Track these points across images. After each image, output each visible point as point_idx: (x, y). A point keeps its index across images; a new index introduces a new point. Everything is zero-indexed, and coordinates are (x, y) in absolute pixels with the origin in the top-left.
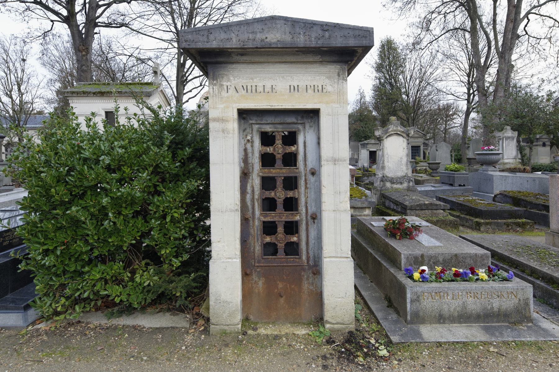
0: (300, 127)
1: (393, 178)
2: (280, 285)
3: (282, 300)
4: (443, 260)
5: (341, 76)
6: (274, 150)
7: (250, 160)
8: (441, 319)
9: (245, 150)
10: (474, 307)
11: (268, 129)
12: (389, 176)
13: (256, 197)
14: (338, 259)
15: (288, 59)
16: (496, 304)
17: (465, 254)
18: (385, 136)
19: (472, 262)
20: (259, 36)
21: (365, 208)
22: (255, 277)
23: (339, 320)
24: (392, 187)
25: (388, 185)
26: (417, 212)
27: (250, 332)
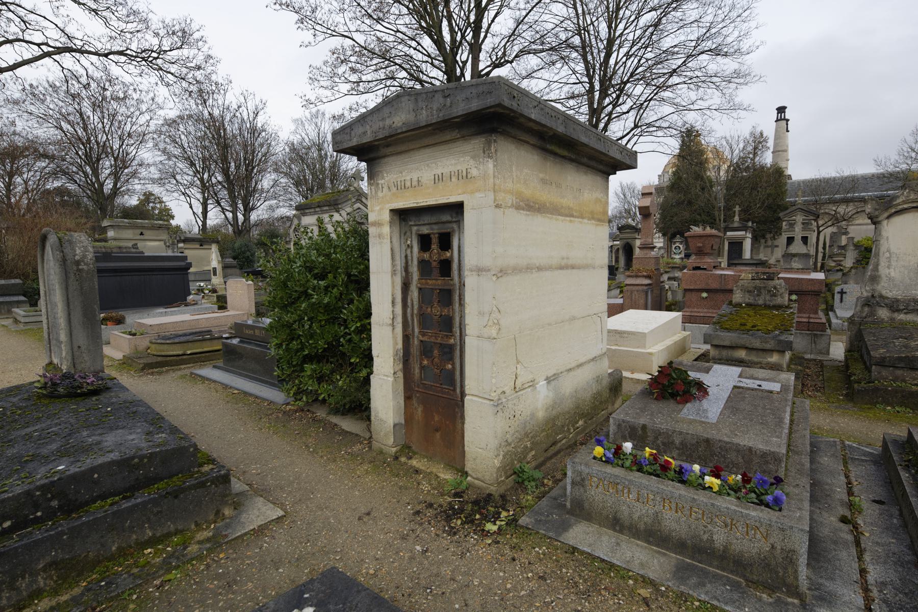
0: (455, 226)
1: (897, 301)
2: (436, 418)
3: (438, 435)
4: (682, 443)
5: (487, 153)
6: (430, 257)
7: (410, 269)
8: (616, 524)
9: (406, 256)
10: (674, 526)
11: (425, 230)
12: (890, 295)
13: (415, 312)
14: (480, 400)
15: (427, 141)
16: (720, 537)
17: (727, 443)
18: (886, 215)
19: (741, 460)
20: (388, 122)
21: (773, 351)
22: (414, 401)
23: (480, 476)
24: (892, 319)
25: (883, 313)
26: (899, 372)
27: (403, 459)
